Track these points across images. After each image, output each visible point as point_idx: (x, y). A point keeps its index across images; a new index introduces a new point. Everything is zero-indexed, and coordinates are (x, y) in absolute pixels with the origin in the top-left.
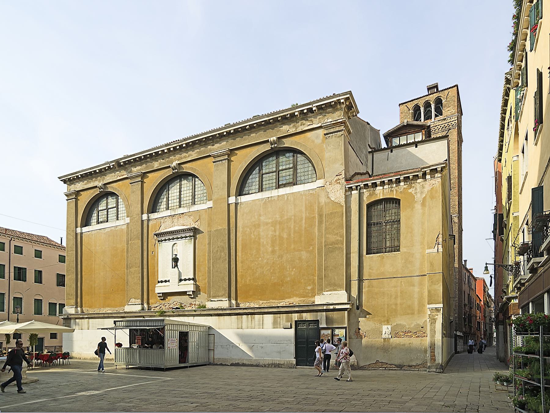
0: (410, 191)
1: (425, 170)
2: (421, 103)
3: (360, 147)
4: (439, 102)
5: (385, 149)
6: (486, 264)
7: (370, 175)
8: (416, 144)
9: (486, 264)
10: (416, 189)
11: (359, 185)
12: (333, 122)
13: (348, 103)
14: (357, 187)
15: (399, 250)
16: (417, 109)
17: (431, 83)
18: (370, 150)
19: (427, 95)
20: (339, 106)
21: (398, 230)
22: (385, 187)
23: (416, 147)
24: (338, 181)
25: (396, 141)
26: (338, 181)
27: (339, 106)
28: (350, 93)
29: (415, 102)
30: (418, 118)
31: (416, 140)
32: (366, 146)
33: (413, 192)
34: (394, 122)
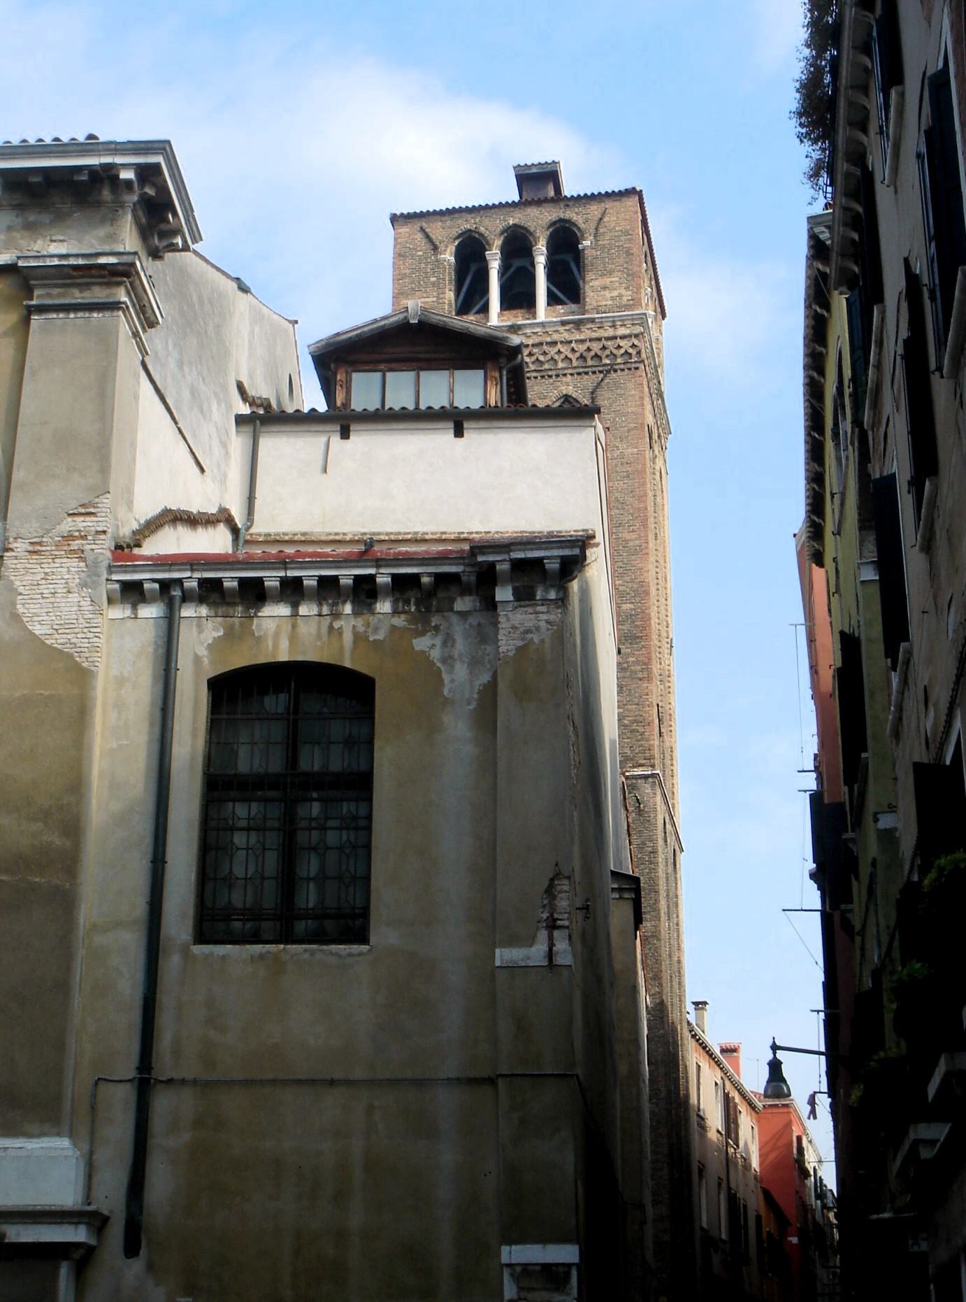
0: (421, 644)
1: (491, 558)
2: (493, 232)
3: (194, 392)
4: (565, 242)
5: (313, 418)
6: (775, 1048)
7: (235, 531)
8: (458, 420)
9: (775, 1048)
10: (448, 641)
11: (179, 582)
12: (72, 261)
13: (150, 191)
14: (165, 585)
15: (361, 936)
16: (470, 253)
17: (535, 156)
18: (245, 410)
19: (514, 204)
20: (106, 194)
21: (363, 825)
22: (303, 610)
23: (459, 433)
24: (75, 545)
25: (364, 390)
26: (75, 545)
27: (106, 194)
28: (163, 147)
29: (466, 224)
30: (472, 298)
31: (461, 404)
32: (224, 388)
33: (435, 654)
34: (368, 301)
